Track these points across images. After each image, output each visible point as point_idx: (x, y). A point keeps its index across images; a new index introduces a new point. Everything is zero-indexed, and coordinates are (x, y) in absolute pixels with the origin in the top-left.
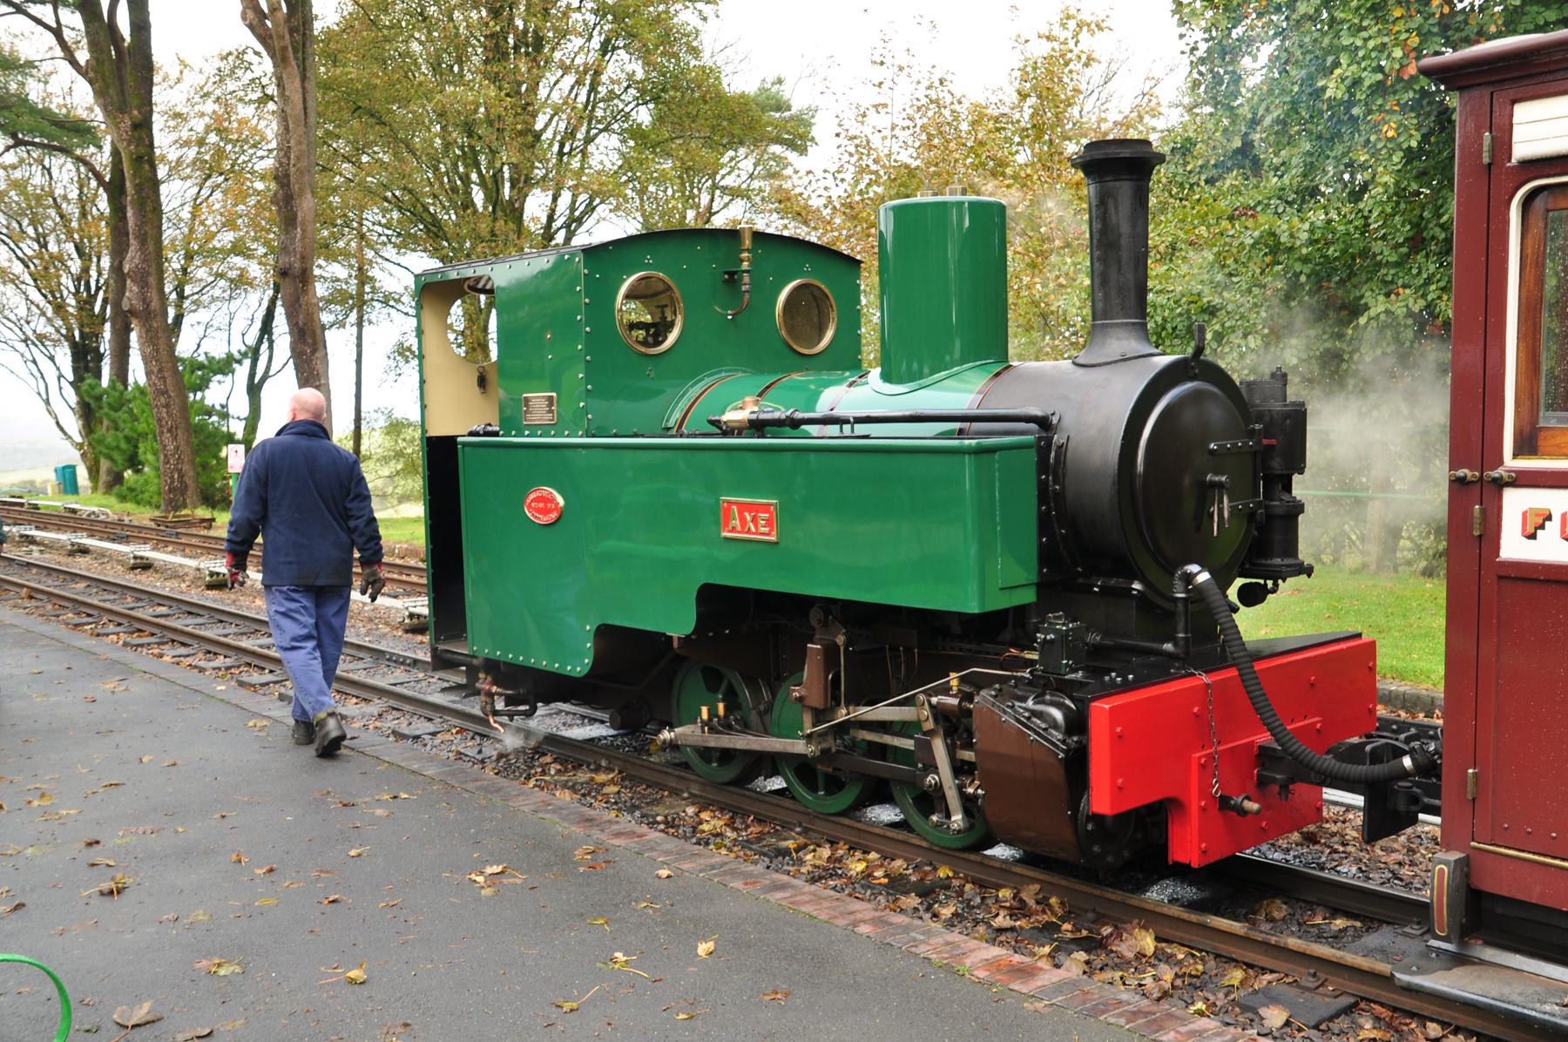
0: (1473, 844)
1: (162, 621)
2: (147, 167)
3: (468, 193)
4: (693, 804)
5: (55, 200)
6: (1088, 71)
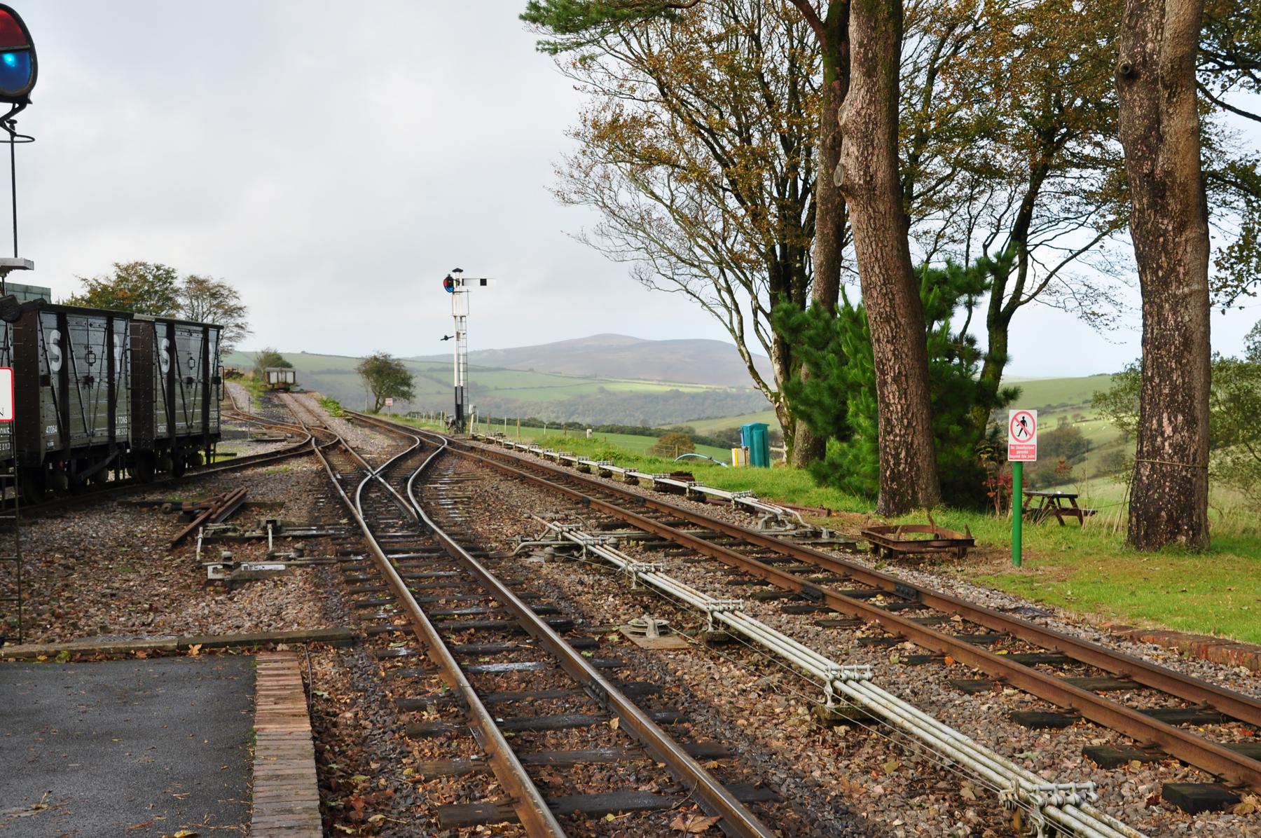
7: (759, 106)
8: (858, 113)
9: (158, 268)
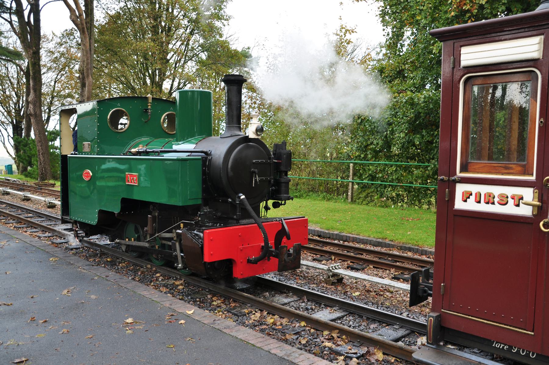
1: (29, 219)
2: (37, 66)
3: (145, 79)
4: (210, 294)
5: (9, 77)
6: (349, 45)
7: (8, 84)
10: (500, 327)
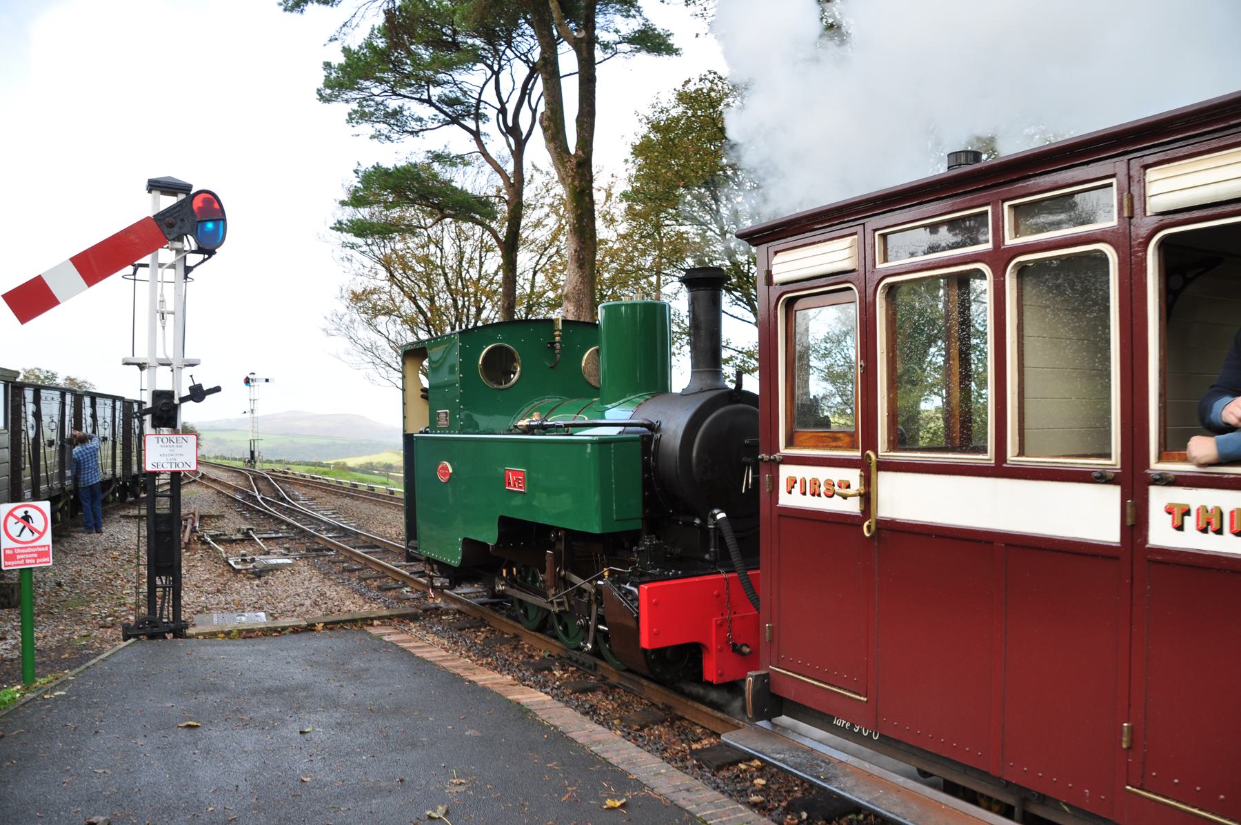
0: (1128, 787)
8: (574, 288)
9: (48, 372)
10: (832, 691)
